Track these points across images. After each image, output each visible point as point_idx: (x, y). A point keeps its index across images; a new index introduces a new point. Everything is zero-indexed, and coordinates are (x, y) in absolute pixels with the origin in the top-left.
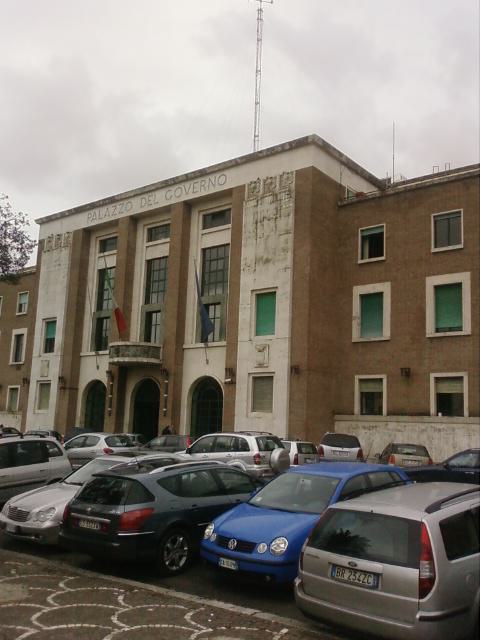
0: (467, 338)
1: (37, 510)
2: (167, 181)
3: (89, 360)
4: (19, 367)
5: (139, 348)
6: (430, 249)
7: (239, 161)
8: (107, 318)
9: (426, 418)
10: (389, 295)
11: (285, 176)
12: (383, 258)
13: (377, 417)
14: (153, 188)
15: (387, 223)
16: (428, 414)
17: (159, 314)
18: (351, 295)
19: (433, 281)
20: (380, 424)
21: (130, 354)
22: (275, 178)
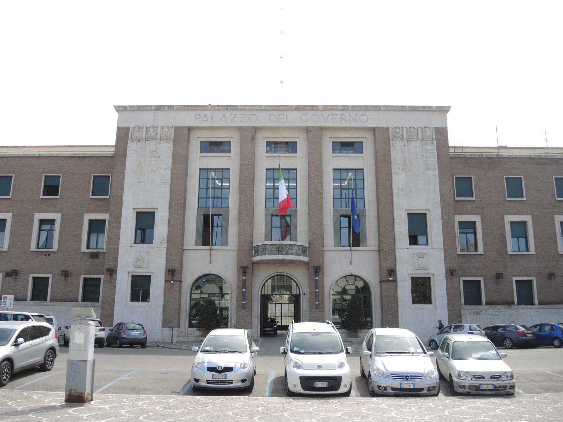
0: (481, 255)
1: (128, 412)
2: (327, 106)
3: (193, 254)
4: (94, 256)
5: (300, 248)
6: (40, 195)
7: (382, 108)
8: (218, 215)
9: (24, 302)
10: (480, 224)
11: (166, 129)
12: (58, 197)
13: (479, 307)
14: (393, 109)
15: (474, 176)
16: (77, 301)
17: (220, 217)
18: (82, 221)
19: (38, 216)
20: (483, 311)
21: (294, 251)
22: (142, 128)
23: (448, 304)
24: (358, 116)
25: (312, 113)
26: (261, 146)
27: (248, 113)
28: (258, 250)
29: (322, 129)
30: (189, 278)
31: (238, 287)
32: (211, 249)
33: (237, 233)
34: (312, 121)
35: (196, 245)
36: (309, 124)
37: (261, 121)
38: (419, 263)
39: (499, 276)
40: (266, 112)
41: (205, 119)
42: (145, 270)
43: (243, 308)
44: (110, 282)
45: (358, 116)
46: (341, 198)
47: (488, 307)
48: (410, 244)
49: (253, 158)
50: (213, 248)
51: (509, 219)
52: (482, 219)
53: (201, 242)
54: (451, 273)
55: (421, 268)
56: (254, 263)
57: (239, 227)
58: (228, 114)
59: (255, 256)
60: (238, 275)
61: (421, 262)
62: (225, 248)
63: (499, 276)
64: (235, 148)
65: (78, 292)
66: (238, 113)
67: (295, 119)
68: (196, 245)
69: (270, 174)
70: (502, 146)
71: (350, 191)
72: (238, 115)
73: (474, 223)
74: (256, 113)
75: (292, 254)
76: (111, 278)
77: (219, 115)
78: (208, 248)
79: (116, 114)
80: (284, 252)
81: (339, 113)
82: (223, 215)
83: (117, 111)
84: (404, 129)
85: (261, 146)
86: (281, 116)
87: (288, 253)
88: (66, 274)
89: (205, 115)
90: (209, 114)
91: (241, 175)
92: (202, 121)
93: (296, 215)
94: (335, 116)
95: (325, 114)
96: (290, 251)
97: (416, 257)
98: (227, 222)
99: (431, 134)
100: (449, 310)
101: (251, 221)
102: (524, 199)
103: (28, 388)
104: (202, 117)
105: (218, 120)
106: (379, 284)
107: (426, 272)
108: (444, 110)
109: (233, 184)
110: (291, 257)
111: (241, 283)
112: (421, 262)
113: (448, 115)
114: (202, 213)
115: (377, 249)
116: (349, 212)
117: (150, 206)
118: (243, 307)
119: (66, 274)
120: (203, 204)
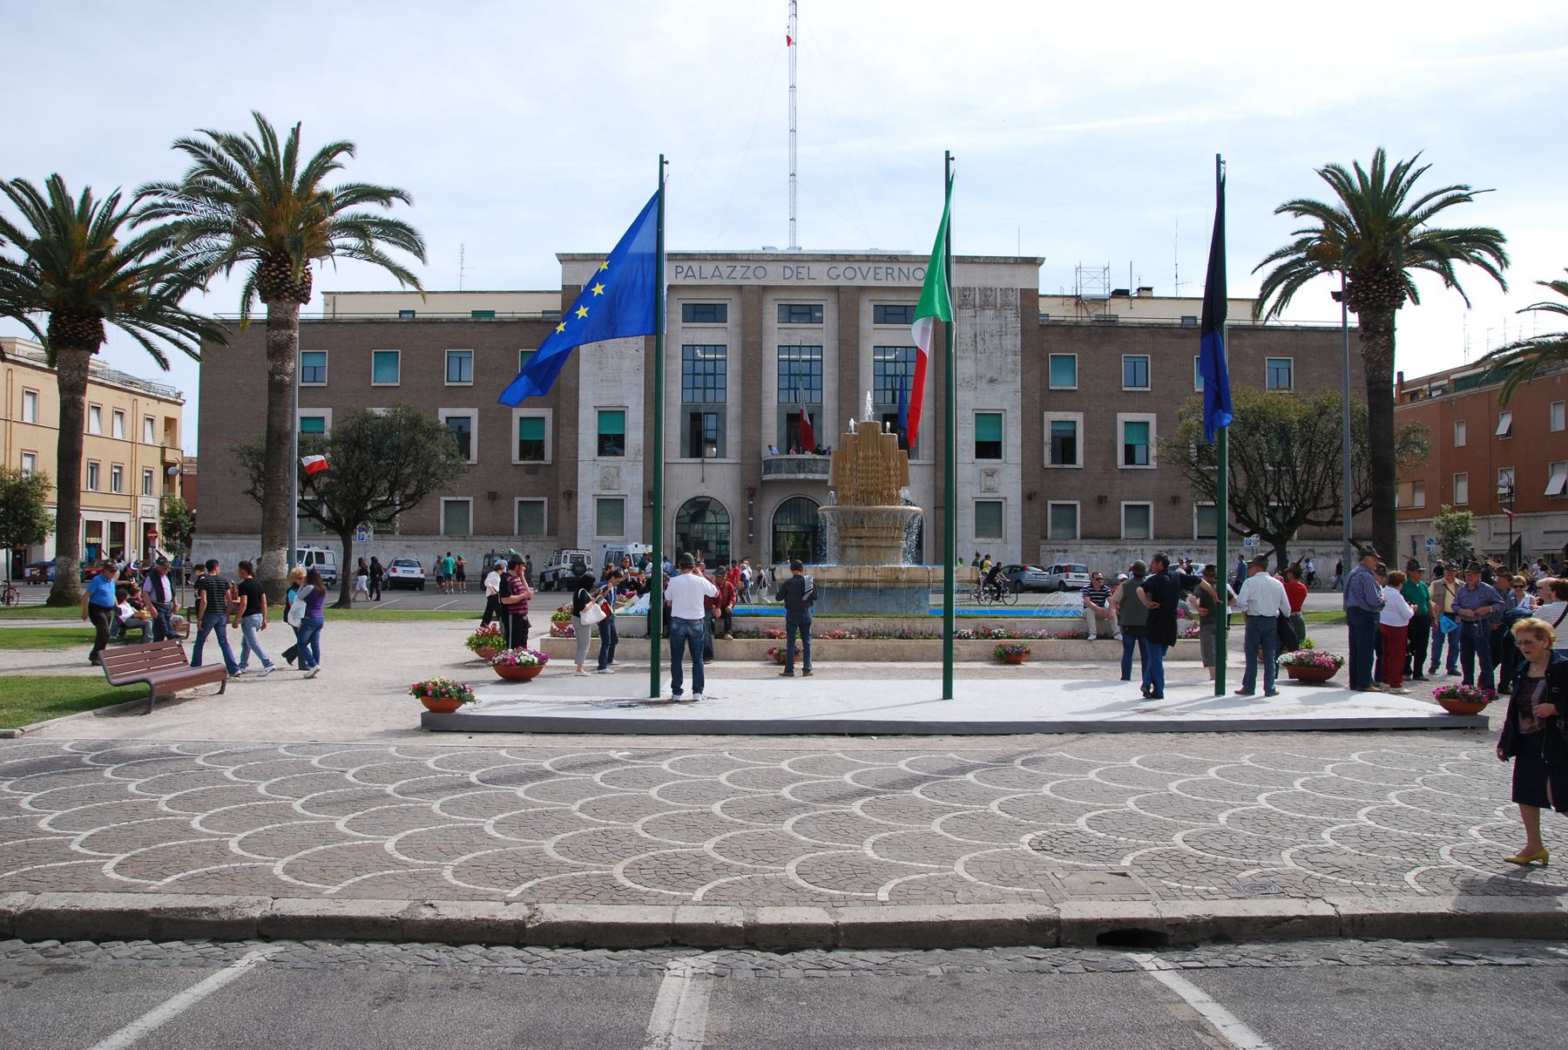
3: (677, 469)
21: (819, 469)
23: (1023, 537)
24: (911, 270)
25: (846, 265)
26: (771, 312)
27: (753, 265)
28: (770, 466)
29: (861, 289)
30: (673, 503)
31: (743, 515)
32: (703, 463)
33: (740, 439)
34: (845, 277)
35: (682, 456)
36: (841, 282)
37: (774, 276)
38: (988, 483)
39: (1101, 500)
40: (779, 263)
41: (690, 273)
42: (616, 493)
43: (750, 543)
44: (569, 509)
45: (911, 270)
46: (790, 389)
47: (1084, 541)
48: (977, 457)
49: (760, 333)
50: (707, 460)
51: (1123, 417)
52: (1085, 418)
53: (688, 454)
54: (1029, 497)
55: (989, 490)
56: (764, 482)
57: (743, 431)
58: (724, 267)
59: (765, 473)
60: (742, 498)
61: (990, 482)
62: (723, 460)
63: (1101, 500)
64: (733, 315)
65: (513, 521)
66: (738, 265)
67: (820, 275)
68: (682, 456)
69: (689, 351)
70: (1396, 333)
71: (898, 379)
72: (738, 268)
73: (1146, 424)
74: (763, 264)
75: (817, 472)
76: (568, 501)
77: (708, 268)
78: (699, 460)
79: (559, 266)
80: (807, 470)
81: (884, 265)
82: (720, 414)
83: (561, 261)
84: (998, 290)
85: (771, 312)
86: (800, 270)
87: (811, 472)
88: (493, 496)
89: (864, 278)
90: (695, 265)
91: (743, 358)
92: (686, 276)
93: (821, 414)
94: (877, 271)
95: (865, 267)
96: (814, 468)
97: (984, 476)
98: (724, 424)
99: (1015, 299)
100: (1023, 546)
101: (758, 425)
102: (1148, 389)
103: (80, 718)
104: (685, 270)
105: (708, 274)
106: (932, 510)
107: (996, 495)
108: (1035, 262)
109: (733, 368)
110: (784, 476)
111: (746, 510)
112: (990, 482)
113: (1041, 268)
114: (689, 411)
115: (933, 462)
116: (895, 411)
117: (618, 403)
118: (750, 541)
119: (493, 496)
120: (688, 399)
